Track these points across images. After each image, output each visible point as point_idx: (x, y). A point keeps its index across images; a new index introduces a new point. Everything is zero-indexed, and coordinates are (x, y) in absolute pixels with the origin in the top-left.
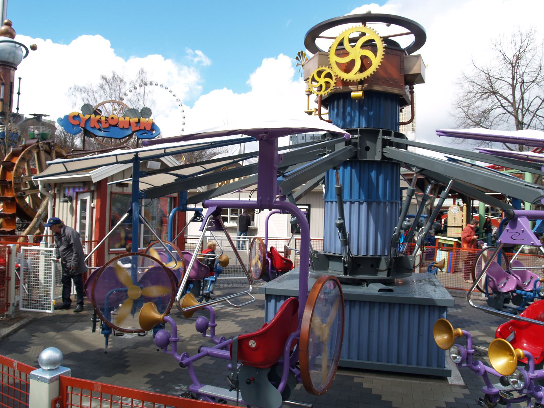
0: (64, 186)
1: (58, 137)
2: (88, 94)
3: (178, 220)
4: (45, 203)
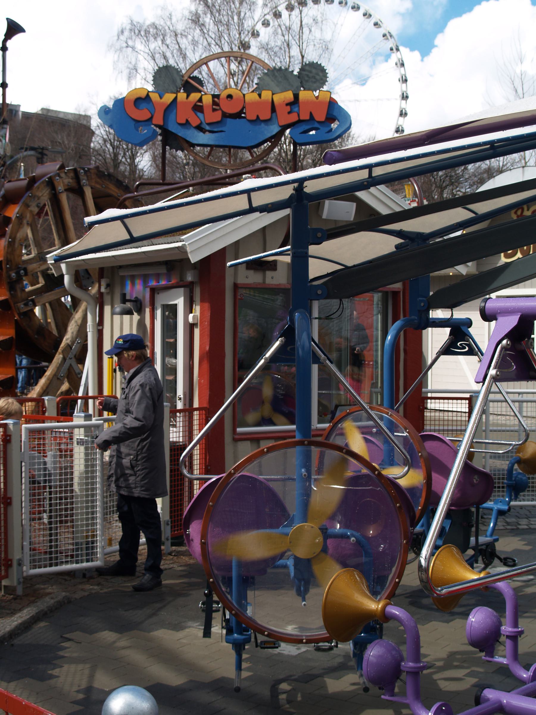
0: (122, 273)
1: (98, 152)
2: (163, 41)
3: (405, 351)
4: (78, 316)
